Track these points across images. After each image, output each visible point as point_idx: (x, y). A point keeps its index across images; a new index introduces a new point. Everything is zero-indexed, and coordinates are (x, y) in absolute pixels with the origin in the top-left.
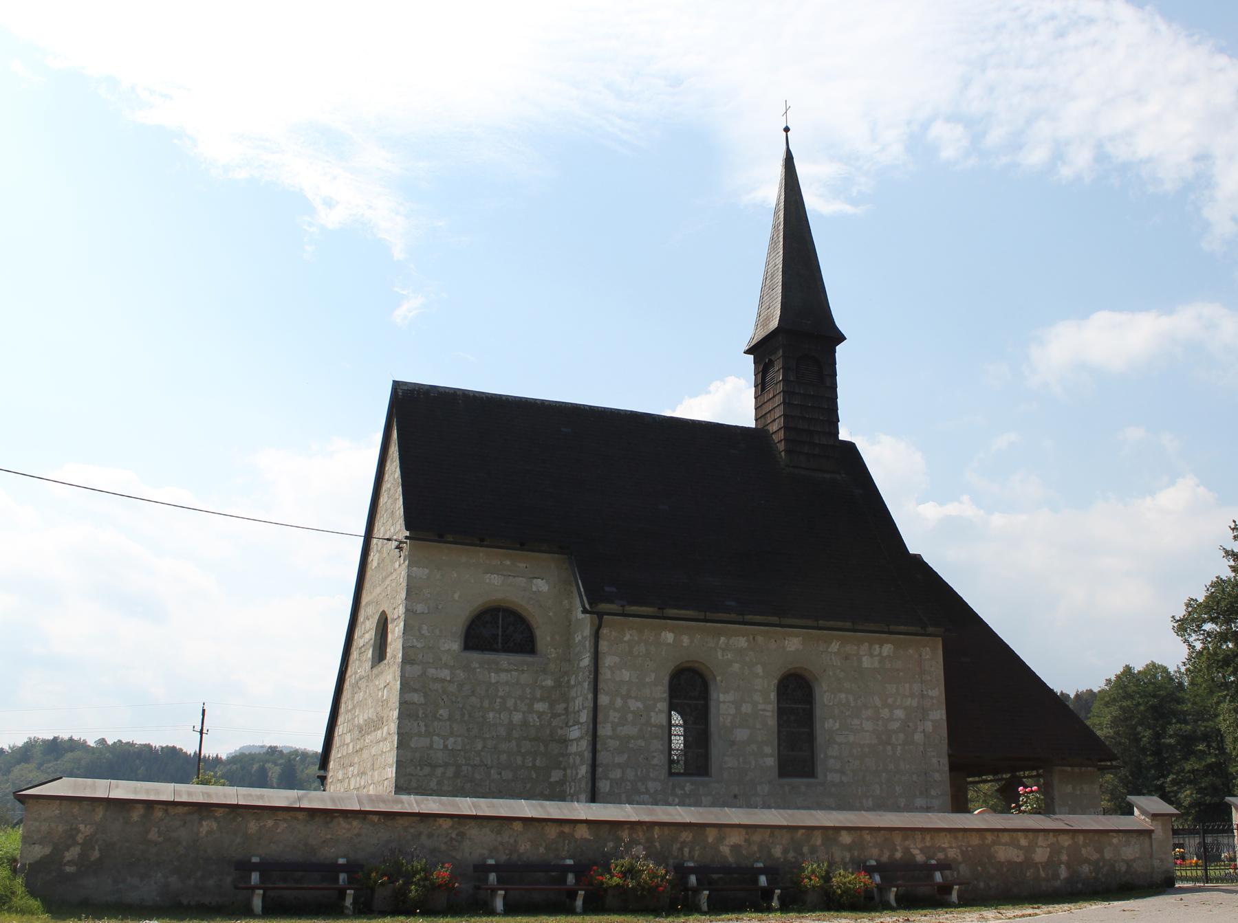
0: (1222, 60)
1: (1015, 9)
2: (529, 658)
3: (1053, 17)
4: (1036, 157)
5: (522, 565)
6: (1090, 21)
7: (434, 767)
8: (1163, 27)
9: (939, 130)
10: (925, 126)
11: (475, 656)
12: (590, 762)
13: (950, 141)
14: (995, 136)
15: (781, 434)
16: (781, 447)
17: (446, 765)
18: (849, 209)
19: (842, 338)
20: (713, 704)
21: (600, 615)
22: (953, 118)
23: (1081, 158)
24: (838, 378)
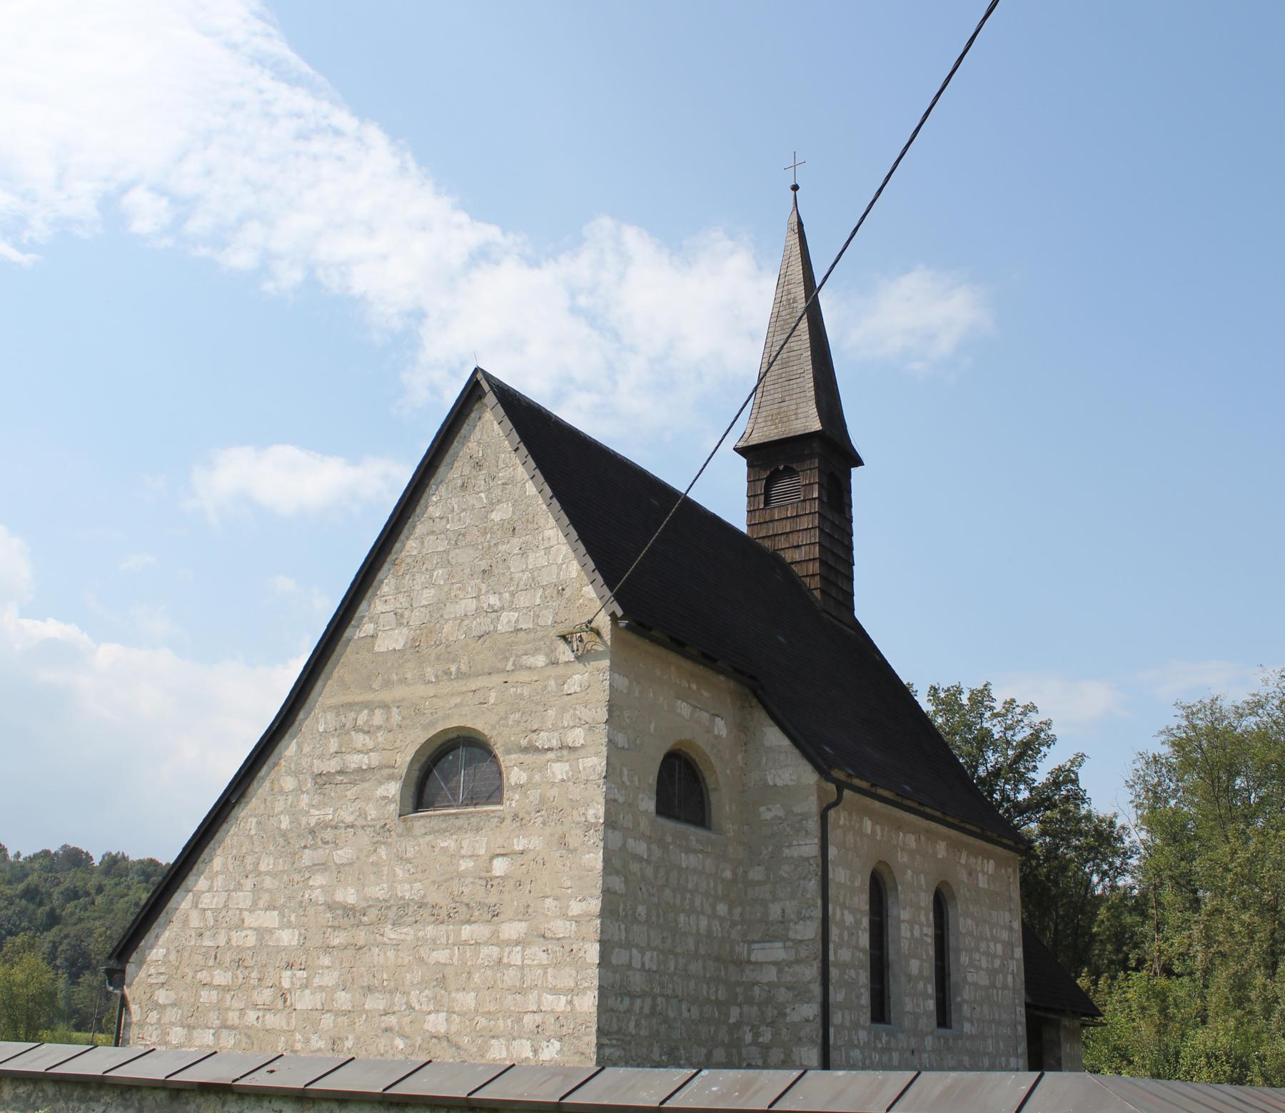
0: (463, 218)
1: (261, 92)
2: (693, 833)
3: (299, 116)
4: (241, 259)
5: (705, 694)
6: (338, 133)
7: (633, 997)
8: (412, 165)
9: (139, 198)
10: (125, 189)
11: (669, 825)
12: (819, 998)
13: (146, 214)
14: (197, 225)
15: (814, 568)
16: (815, 583)
17: (643, 995)
18: (14, 255)
19: (859, 462)
20: (891, 921)
21: (840, 786)
22: (158, 190)
23: (291, 277)
24: (853, 510)
